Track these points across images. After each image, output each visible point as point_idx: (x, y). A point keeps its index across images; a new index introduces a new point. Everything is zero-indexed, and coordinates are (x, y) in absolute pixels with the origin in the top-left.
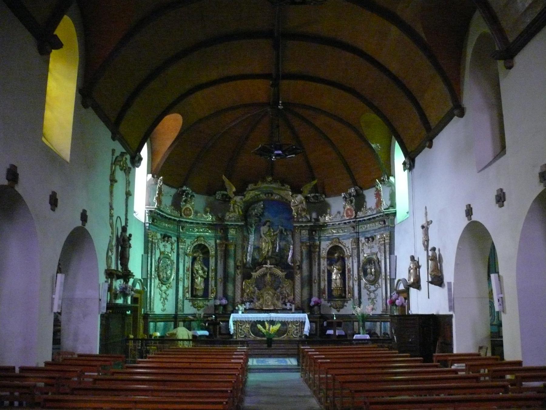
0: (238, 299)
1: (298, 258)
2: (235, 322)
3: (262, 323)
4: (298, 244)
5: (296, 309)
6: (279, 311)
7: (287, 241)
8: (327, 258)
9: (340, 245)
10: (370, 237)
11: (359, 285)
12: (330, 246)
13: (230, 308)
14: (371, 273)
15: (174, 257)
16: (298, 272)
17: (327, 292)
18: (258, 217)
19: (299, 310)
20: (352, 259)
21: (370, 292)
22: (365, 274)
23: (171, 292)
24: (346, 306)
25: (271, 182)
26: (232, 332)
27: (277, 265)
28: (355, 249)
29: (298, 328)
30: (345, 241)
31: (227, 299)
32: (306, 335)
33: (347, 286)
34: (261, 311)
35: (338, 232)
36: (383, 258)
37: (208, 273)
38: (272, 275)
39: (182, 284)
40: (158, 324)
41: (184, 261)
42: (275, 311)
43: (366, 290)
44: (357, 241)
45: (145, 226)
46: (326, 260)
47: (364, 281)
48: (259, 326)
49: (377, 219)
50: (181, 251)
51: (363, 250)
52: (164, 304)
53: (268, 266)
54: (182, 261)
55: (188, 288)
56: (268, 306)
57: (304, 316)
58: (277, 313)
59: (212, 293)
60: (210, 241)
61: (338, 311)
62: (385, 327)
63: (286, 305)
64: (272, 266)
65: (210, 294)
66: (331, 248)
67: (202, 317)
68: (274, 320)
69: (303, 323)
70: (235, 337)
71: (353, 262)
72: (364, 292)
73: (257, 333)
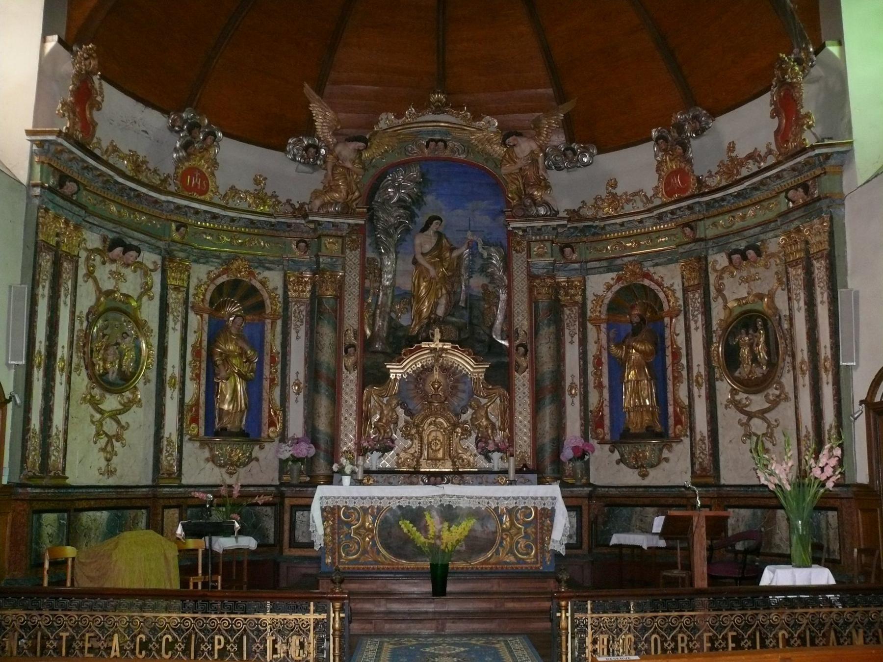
0: (348, 441)
1: (522, 322)
2: (329, 513)
3: (416, 515)
4: (520, 282)
5: (518, 471)
6: (467, 478)
7: (491, 276)
8: (608, 322)
9: (646, 282)
10: (748, 248)
11: (711, 398)
12: (616, 288)
13: (321, 468)
14: (755, 360)
15: (149, 312)
16: (523, 362)
17: (607, 422)
18: (405, 208)
19: (534, 470)
20: (686, 319)
21: (751, 416)
22: (732, 359)
23: (139, 419)
24: (667, 460)
25: (439, 109)
26: (319, 543)
27: (462, 343)
28: (696, 288)
29: (530, 530)
30: (660, 272)
31: (314, 442)
32: (557, 555)
33: (671, 401)
34: (413, 475)
35: (639, 247)
36: (800, 305)
37: (261, 363)
38: (448, 370)
39: (176, 394)
40: (87, 517)
41: (185, 326)
42: (458, 476)
43: (733, 412)
44: (701, 266)
45: (29, 197)
46: (603, 326)
47: (724, 388)
48: (406, 526)
49: (776, 186)
50: (173, 297)
51: (720, 291)
52: (109, 453)
53: (437, 344)
54: (178, 326)
55: (197, 404)
56: (435, 460)
57: (553, 490)
58: (463, 482)
59: (272, 424)
60: (267, 274)
61: (644, 476)
62: (110, 442)
63: (489, 459)
64: (448, 346)
65: (265, 427)
66: (618, 292)
67: (236, 493)
68: (466, 533)
69: (548, 515)
70: (329, 560)
71: (687, 330)
72: (728, 418)
73: (401, 546)
